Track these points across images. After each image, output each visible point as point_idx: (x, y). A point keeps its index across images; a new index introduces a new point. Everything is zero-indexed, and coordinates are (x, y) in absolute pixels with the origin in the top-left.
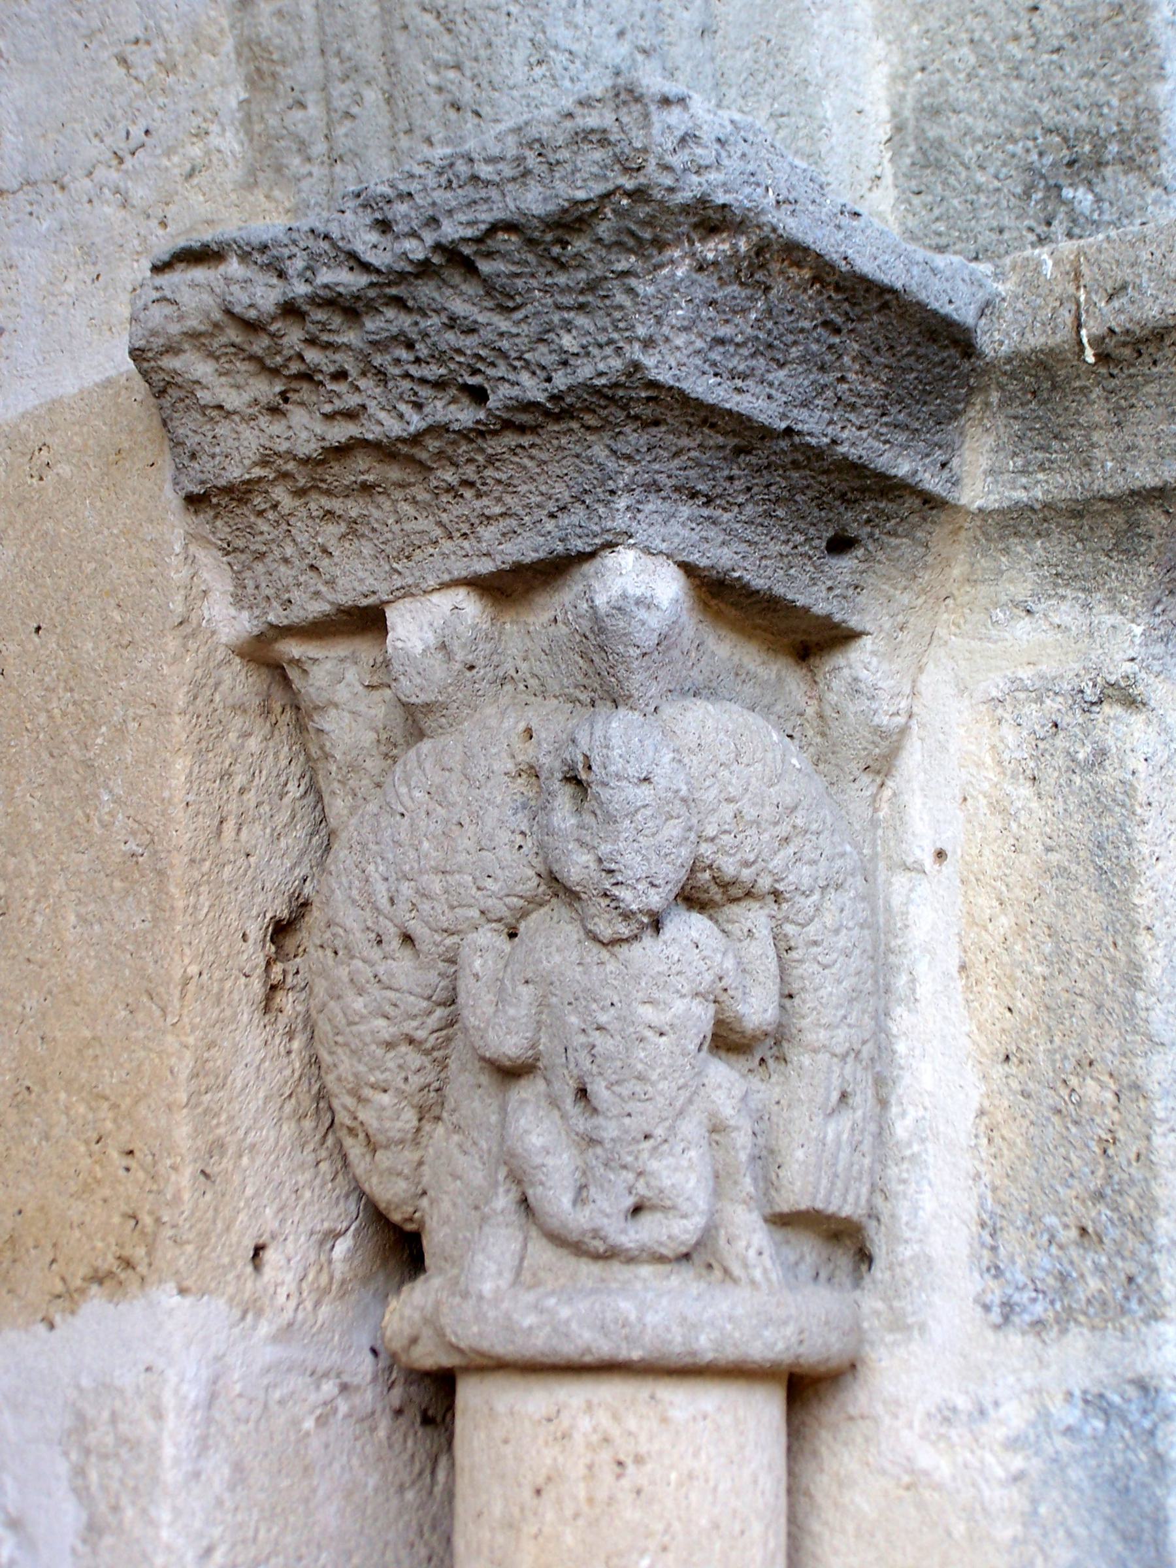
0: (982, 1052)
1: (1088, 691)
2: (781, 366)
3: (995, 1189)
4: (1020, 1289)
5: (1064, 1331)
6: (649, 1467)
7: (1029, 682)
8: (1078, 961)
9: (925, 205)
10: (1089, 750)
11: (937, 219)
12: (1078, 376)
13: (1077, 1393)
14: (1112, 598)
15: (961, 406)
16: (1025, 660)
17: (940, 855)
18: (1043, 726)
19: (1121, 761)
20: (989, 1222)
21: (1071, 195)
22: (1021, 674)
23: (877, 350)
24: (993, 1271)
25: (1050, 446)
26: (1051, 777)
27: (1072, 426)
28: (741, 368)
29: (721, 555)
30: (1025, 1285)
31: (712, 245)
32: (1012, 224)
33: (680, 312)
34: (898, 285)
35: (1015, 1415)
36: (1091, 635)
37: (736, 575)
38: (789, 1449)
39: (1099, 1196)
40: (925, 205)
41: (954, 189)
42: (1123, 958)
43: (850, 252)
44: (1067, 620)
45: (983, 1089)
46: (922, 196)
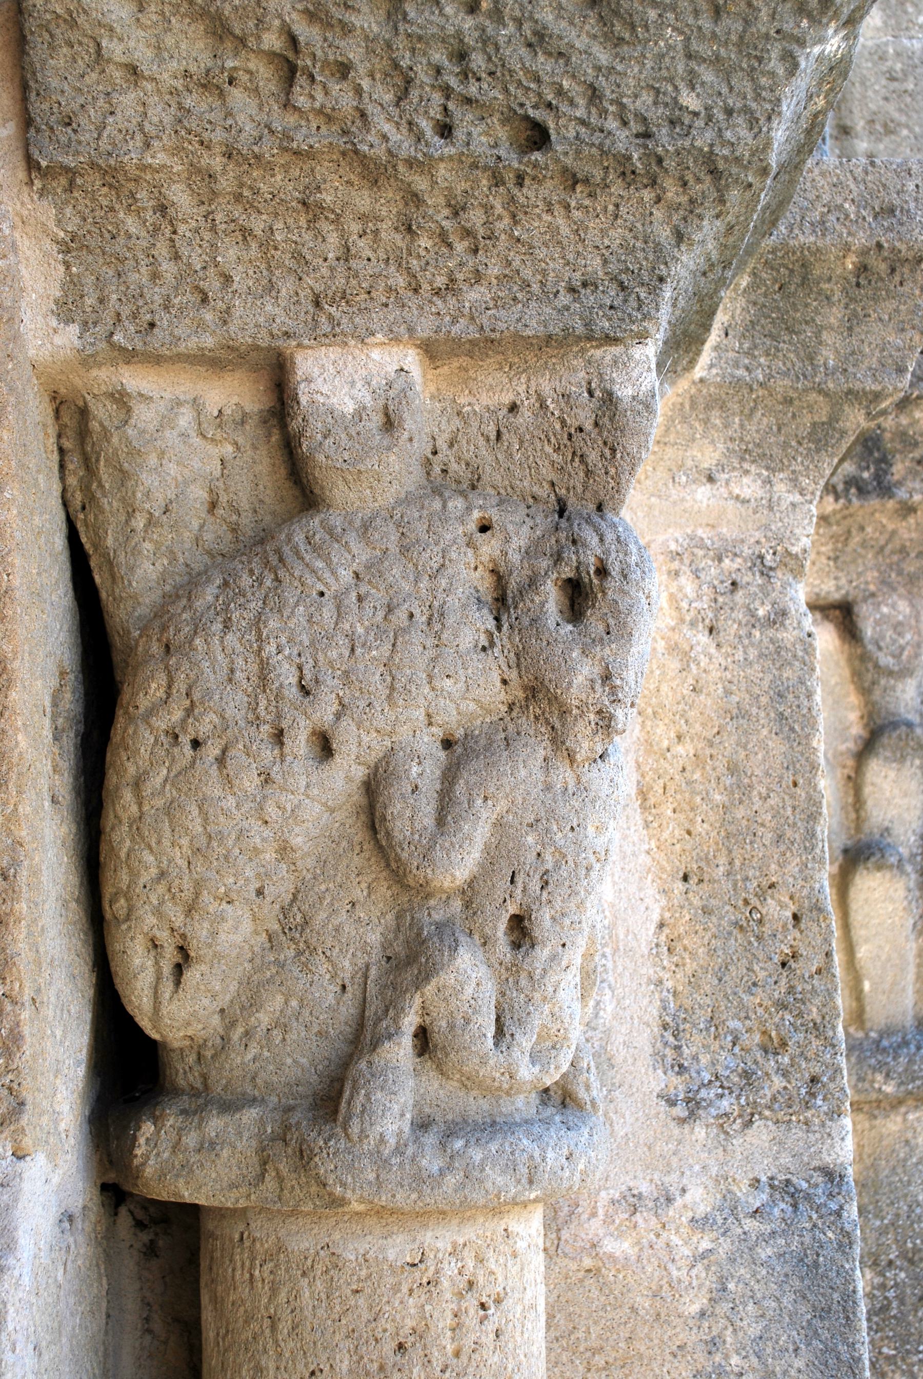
0: (663, 869)
1: (769, 557)
3: (675, 994)
7: (709, 543)
8: (760, 794)
13: (764, 1179)
14: (794, 481)
16: (704, 522)
18: (722, 582)
19: (799, 623)
20: (672, 1024)
22: (700, 532)
24: (676, 1069)
25: (779, 336)
27: (807, 323)
30: (710, 1082)
35: (699, 1198)
36: (771, 508)
39: (782, 1006)
42: (803, 795)
44: (746, 493)
45: (664, 902)
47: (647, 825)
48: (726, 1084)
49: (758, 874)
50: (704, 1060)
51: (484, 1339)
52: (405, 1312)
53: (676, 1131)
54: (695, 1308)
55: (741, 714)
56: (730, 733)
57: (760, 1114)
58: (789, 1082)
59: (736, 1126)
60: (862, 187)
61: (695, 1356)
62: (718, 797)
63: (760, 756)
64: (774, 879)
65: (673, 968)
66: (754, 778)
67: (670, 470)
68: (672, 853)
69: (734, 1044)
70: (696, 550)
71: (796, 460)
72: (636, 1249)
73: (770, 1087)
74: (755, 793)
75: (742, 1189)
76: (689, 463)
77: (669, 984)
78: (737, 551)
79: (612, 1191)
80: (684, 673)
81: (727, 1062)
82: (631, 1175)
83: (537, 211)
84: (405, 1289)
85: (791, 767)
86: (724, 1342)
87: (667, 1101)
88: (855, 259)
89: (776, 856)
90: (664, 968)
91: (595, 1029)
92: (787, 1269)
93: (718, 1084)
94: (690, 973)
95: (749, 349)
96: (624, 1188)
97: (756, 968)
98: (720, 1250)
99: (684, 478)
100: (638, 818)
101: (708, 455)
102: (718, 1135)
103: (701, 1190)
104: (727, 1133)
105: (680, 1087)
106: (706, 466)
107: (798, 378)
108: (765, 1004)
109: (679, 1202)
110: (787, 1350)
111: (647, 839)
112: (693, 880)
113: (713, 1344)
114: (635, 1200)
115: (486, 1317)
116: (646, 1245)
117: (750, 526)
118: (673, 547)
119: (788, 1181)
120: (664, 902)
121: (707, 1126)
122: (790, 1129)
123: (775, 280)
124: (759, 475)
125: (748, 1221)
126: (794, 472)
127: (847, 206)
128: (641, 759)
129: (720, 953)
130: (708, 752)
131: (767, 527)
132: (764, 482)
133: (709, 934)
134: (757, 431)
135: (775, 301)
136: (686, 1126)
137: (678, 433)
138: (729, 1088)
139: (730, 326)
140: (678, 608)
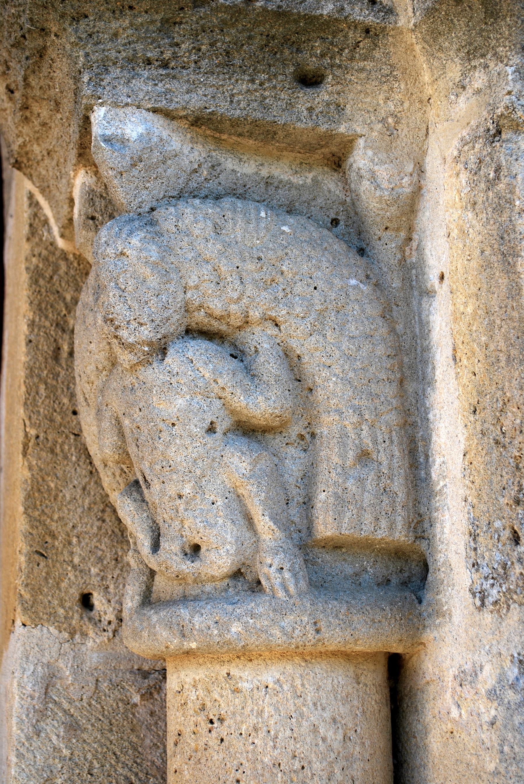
6: (226, 723)
39: (518, 502)
51: (210, 743)
71: (490, 38)
101: (454, 71)
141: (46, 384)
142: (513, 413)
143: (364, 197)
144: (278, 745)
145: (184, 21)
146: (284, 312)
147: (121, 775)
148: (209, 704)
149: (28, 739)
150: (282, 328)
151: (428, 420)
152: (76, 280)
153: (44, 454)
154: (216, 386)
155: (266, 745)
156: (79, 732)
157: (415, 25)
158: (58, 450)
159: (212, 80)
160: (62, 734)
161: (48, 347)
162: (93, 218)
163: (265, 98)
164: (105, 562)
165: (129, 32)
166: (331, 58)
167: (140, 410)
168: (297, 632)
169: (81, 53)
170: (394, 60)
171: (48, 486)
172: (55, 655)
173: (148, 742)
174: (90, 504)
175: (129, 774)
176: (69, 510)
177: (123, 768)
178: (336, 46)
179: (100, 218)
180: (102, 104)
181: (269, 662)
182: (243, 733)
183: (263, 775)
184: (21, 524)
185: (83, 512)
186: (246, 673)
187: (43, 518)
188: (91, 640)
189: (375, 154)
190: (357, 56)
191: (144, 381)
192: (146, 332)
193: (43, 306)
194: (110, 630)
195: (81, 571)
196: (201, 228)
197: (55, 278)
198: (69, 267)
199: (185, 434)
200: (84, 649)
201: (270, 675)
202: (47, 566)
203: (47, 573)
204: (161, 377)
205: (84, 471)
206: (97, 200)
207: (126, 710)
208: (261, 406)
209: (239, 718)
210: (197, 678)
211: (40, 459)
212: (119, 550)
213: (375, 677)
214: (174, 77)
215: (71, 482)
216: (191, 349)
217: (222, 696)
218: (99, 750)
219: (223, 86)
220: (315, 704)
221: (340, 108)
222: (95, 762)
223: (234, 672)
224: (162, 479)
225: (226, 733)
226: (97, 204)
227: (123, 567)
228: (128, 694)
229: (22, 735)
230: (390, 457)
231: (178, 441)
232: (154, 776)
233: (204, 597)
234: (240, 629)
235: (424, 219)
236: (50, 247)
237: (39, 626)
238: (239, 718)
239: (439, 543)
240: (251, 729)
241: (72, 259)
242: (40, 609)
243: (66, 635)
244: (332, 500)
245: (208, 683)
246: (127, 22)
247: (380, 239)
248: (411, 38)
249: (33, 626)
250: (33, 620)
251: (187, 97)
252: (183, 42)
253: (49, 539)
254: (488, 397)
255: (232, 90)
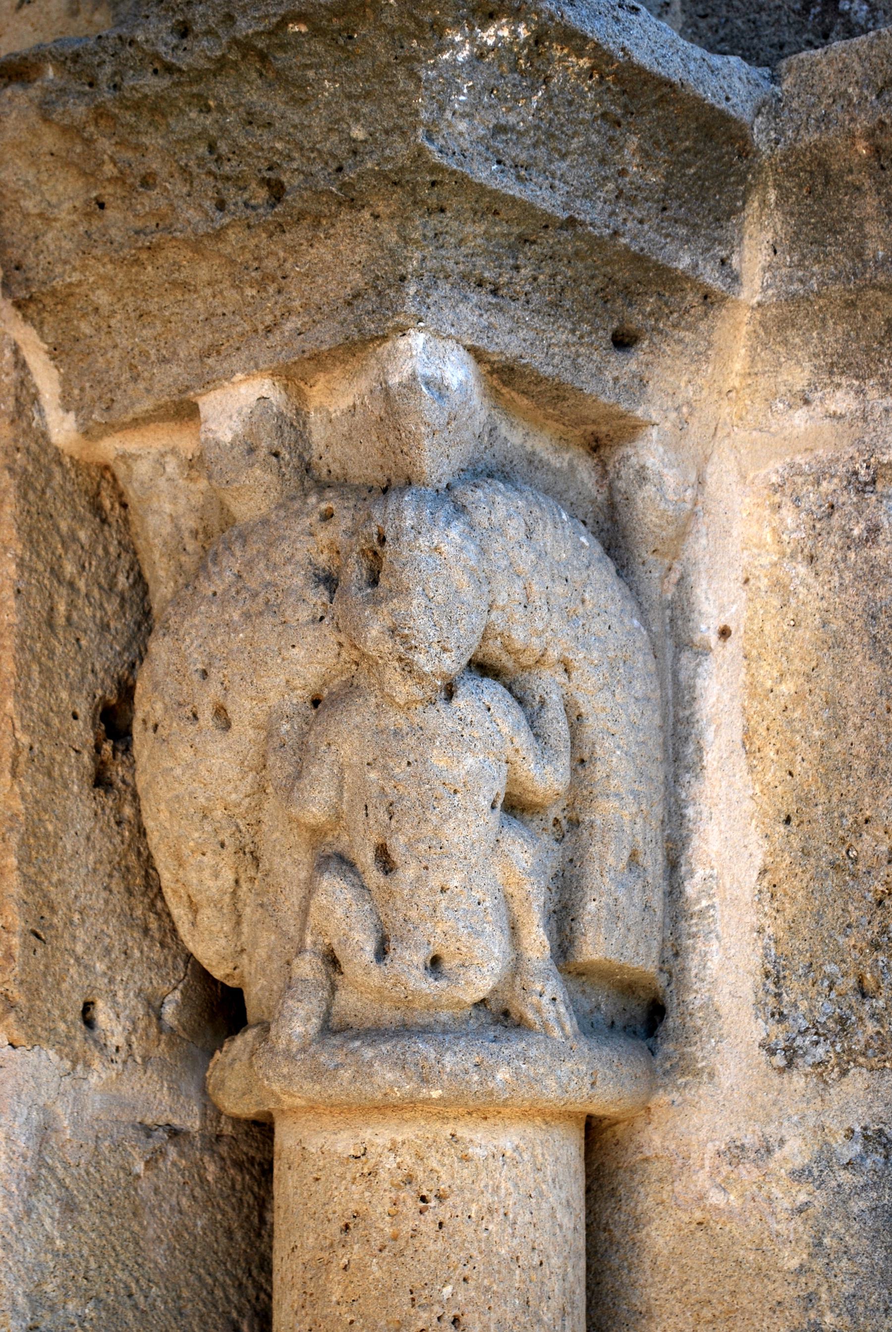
2: (563, 157)
4: (803, 1033)
5: (844, 1073)
6: (449, 1202)
8: (855, 724)
9: (711, 28)
10: (862, 526)
11: (722, 40)
12: (851, 171)
13: (858, 1129)
15: (739, 204)
17: (725, 633)
20: (773, 972)
21: (847, 7)
22: (799, 459)
23: (657, 143)
24: (777, 1017)
25: (824, 240)
26: (828, 554)
27: (846, 219)
28: (523, 156)
29: (509, 344)
31: (491, 31)
32: (792, 39)
33: (462, 98)
34: (675, 79)
35: (796, 1150)
36: (865, 419)
37: (524, 361)
38: (588, 1190)
39: (876, 946)
40: (711, 28)
41: (738, 10)
43: (627, 43)
45: (766, 847)
46: (709, 19)
47: (752, 769)
48: (821, 1031)
49: (853, 809)
50: (803, 1006)
51: (423, 1228)
52: (349, 1196)
53: (776, 1081)
54: (794, 1263)
55: (838, 643)
56: (826, 664)
57: (855, 1061)
58: (882, 1026)
59: (834, 1075)
60: (867, 65)
61: (793, 1312)
62: (816, 733)
63: (853, 685)
64: (868, 813)
65: (774, 914)
66: (849, 709)
67: (767, 400)
68: (774, 796)
69: (831, 989)
70: (796, 478)
71: (882, 362)
72: (740, 1201)
73: (864, 1032)
74: (850, 724)
75: (838, 1140)
76: (783, 389)
77: (770, 931)
78: (833, 471)
79: (717, 1143)
80: (785, 609)
81: (825, 1009)
82: (735, 1127)
83: (303, 247)
84: (349, 1176)
85: (884, 693)
86: (820, 1299)
87: (768, 1050)
88: (865, 144)
89: (870, 789)
90: (766, 914)
91: (703, 980)
92: (879, 1224)
93: (814, 1031)
94: (789, 918)
95: (800, 260)
96: (728, 1139)
97: (851, 908)
98: (816, 1203)
99: (781, 406)
100: (743, 764)
101: (798, 376)
102: (817, 1085)
103: (799, 1141)
104: (825, 1082)
105: (781, 1036)
106: (799, 388)
107: (849, 279)
108: (859, 945)
109: (777, 1154)
110: (878, 1309)
111: (751, 784)
112: (795, 822)
113: (810, 1299)
114: (738, 1151)
115: (427, 1208)
116: (749, 1197)
117: (845, 442)
118: (775, 479)
119: (880, 1130)
120: (766, 847)
121: (806, 1075)
122: (883, 1076)
123: (801, 187)
124: (851, 386)
125: (842, 1173)
126: (882, 375)
127: (850, 90)
128: (746, 703)
129: (817, 895)
130: (807, 687)
131: (861, 440)
132: (857, 393)
133: (808, 876)
134: (836, 341)
135: (809, 206)
136: (785, 1075)
137: (763, 361)
138: (824, 1035)
139: (776, 242)
140: (780, 542)
141: (40, 664)
142: (875, 837)
143: (640, 505)
144: (517, 1232)
145: (539, 241)
146: (581, 656)
147: (121, 1280)
148: (421, 1175)
149: (18, 1221)
150: (573, 676)
151: (683, 816)
152: (74, 500)
153: (40, 777)
154: (511, 746)
155: (504, 1231)
156: (76, 1214)
157: (760, 305)
158: (56, 774)
159: (536, 322)
160: (57, 1215)
161: (42, 606)
162: (276, 455)
163: (579, 356)
164: (113, 956)
165: (479, 241)
166: (657, 320)
167: (409, 764)
168: (573, 1083)
169: (418, 255)
170: (715, 337)
171: (46, 829)
172: (53, 1094)
173: (151, 1232)
174: (95, 863)
175: (129, 1280)
176: (70, 869)
177: (123, 1270)
178: (668, 307)
179: (287, 457)
180: (420, 330)
181: (507, 1122)
182: (473, 1215)
183: (499, 1272)
184: (14, 884)
185: (87, 875)
186: (479, 1135)
187: (40, 879)
188: (95, 1074)
189: (665, 452)
190: (683, 323)
191: (421, 725)
192: (449, 662)
193: (35, 536)
194: (119, 1061)
195: (86, 967)
196: (515, 529)
197: (49, 492)
198: (64, 478)
199: (470, 807)
200: (85, 1087)
201: (510, 1138)
202: (45, 955)
203: (47, 967)
204: (450, 724)
205: (87, 810)
206: (286, 429)
207: (129, 1183)
208: (547, 779)
209: (468, 1196)
210: (399, 1139)
211: (36, 785)
212: (129, 938)
213: (565, 1151)
214: (501, 310)
215: (74, 827)
216: (486, 691)
217: (444, 1165)
218: (97, 1242)
219: (544, 331)
220: (554, 1181)
221: (643, 383)
222: (92, 1259)
223: (463, 1132)
224: (424, 864)
225: (448, 1215)
226: (285, 435)
227: (133, 965)
228: (131, 1160)
229: (10, 1215)
230: (653, 862)
231: (460, 815)
232: (157, 1284)
233: (438, 1029)
234: (507, 1076)
235: (696, 547)
236: (41, 440)
237: (37, 1048)
238: (468, 1196)
239: (694, 980)
240: (484, 1210)
241: (69, 465)
242: (39, 1021)
243: (68, 1064)
244: (604, 913)
245: (420, 1146)
246: (483, 228)
247: (643, 563)
248: (745, 315)
249: (29, 1048)
250: (29, 1038)
251: (507, 338)
252: (525, 266)
253: (46, 913)
254: (820, 807)
255: (551, 338)
